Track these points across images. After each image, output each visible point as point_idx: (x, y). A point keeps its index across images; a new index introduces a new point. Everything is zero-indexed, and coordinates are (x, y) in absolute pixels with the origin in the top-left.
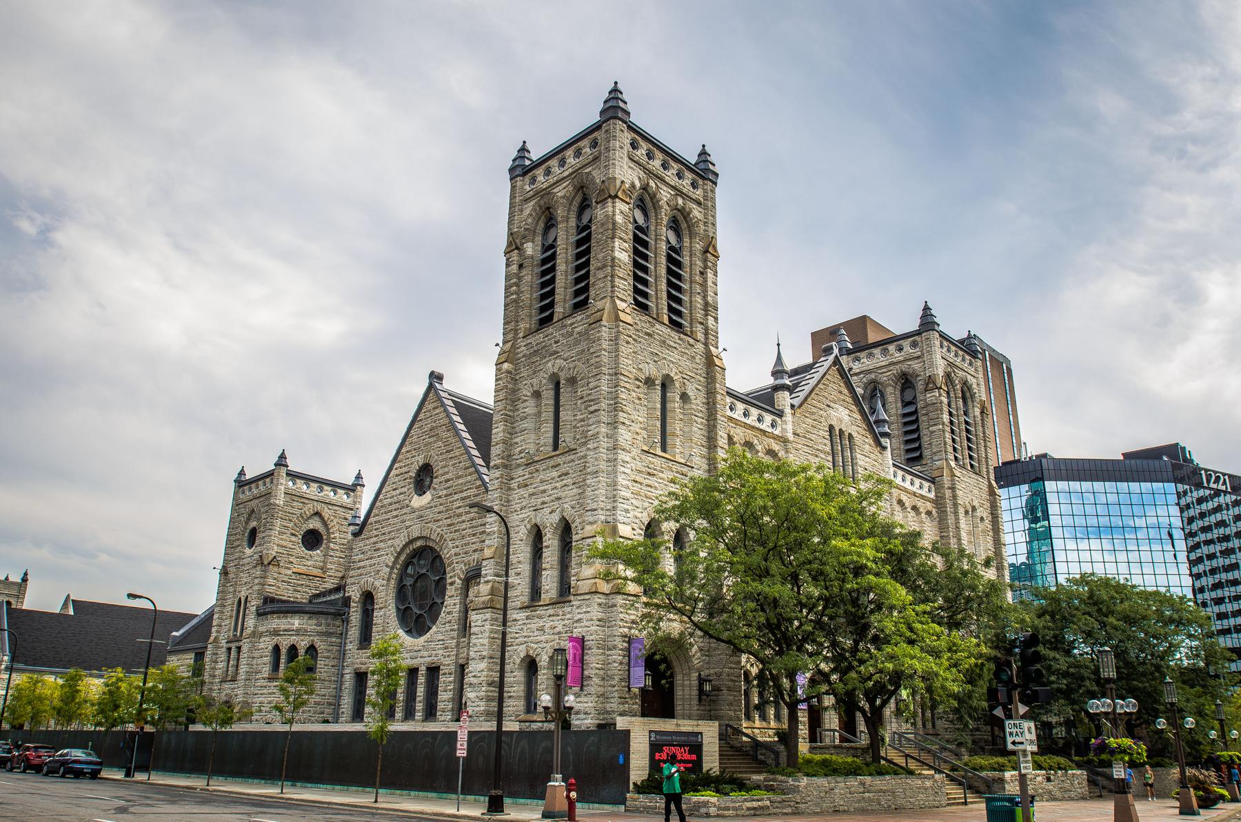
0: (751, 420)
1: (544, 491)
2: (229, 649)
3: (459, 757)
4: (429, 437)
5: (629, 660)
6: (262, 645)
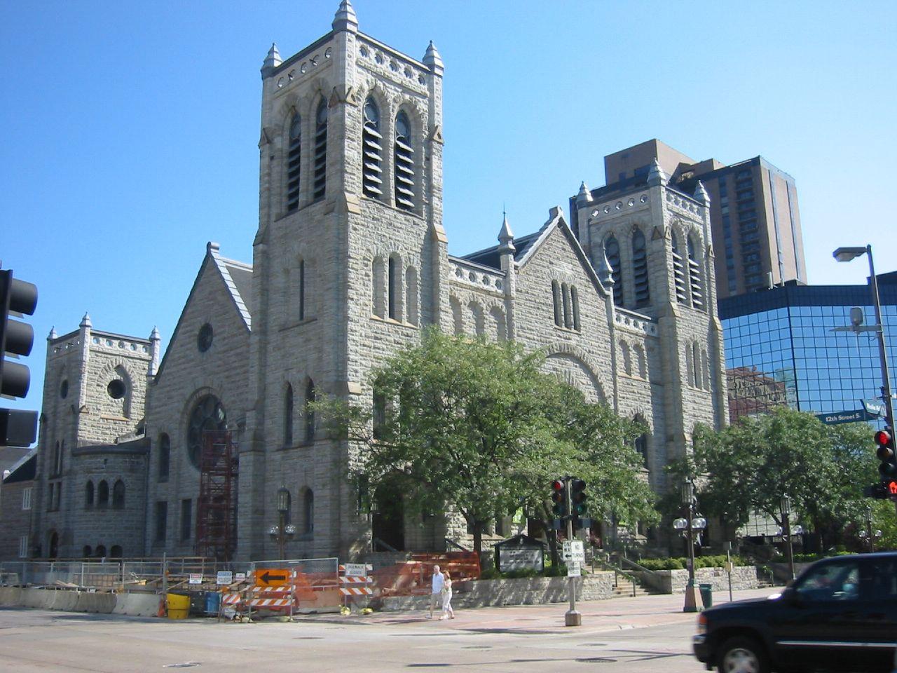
2: (52, 485)
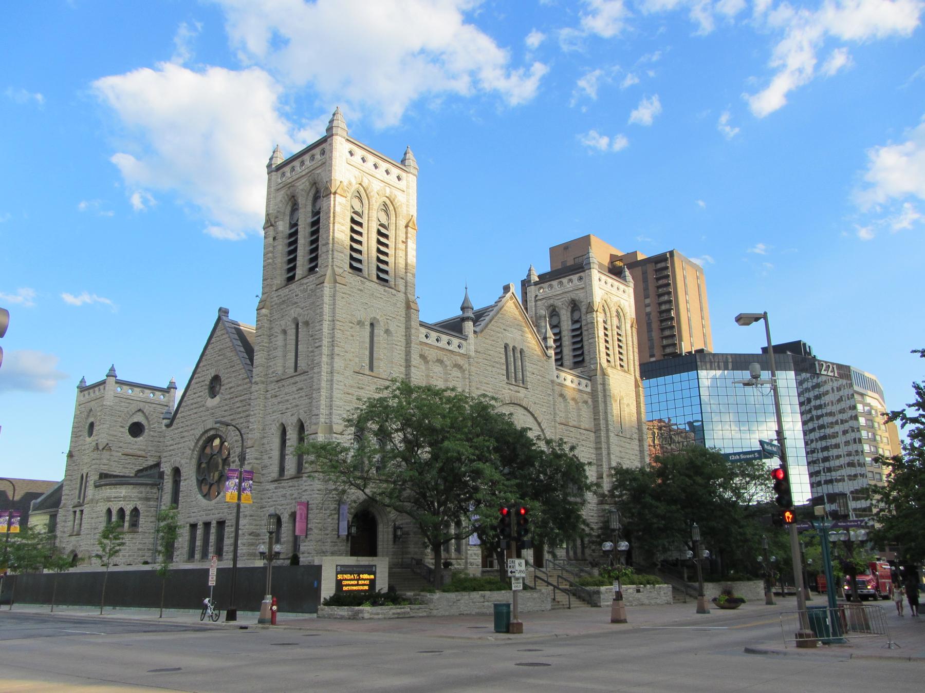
0: (443, 344)
1: (288, 401)
2: (75, 512)
3: (211, 586)
4: (219, 356)
5: (339, 516)
6: (98, 509)
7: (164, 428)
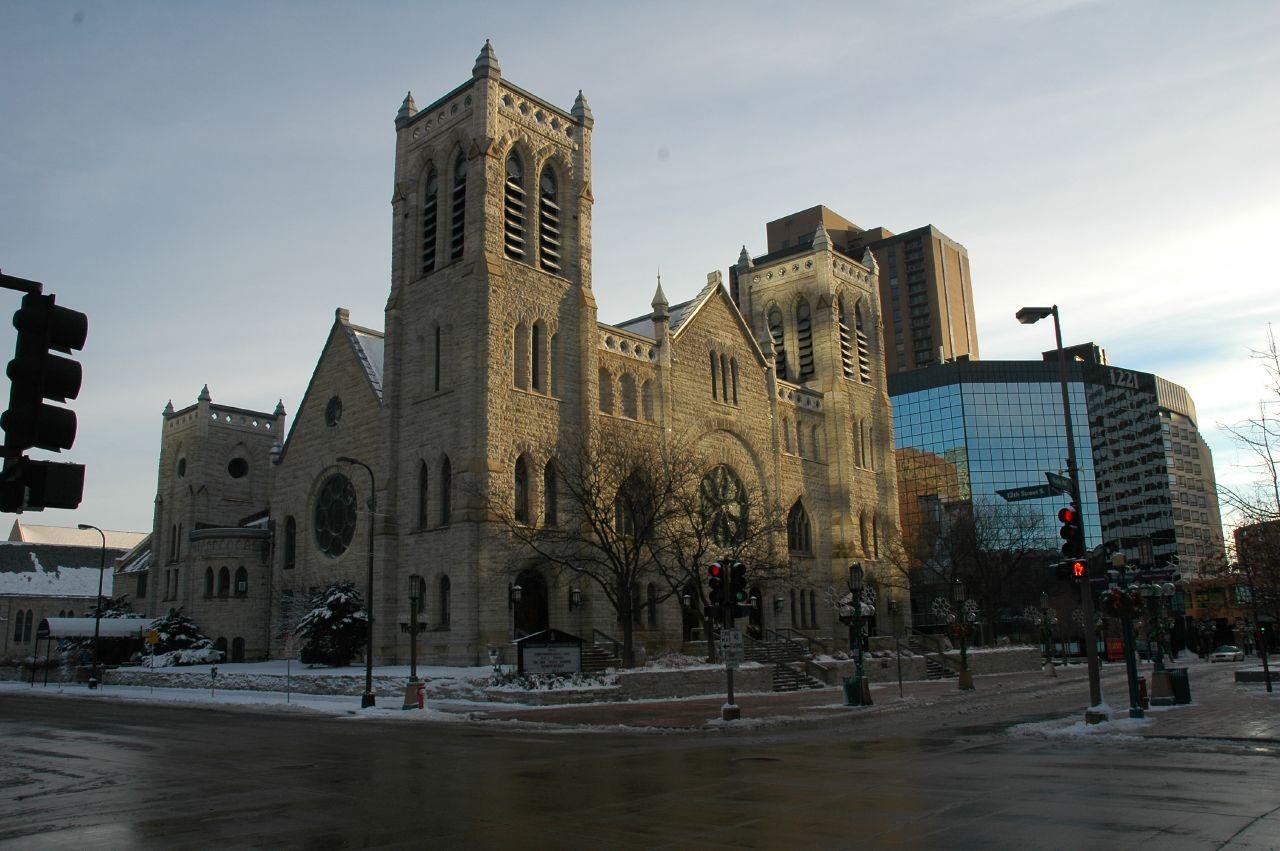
2: (169, 572)
7: (272, 465)
